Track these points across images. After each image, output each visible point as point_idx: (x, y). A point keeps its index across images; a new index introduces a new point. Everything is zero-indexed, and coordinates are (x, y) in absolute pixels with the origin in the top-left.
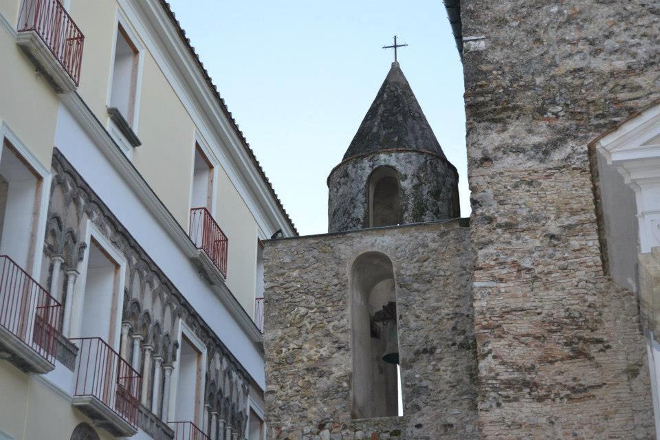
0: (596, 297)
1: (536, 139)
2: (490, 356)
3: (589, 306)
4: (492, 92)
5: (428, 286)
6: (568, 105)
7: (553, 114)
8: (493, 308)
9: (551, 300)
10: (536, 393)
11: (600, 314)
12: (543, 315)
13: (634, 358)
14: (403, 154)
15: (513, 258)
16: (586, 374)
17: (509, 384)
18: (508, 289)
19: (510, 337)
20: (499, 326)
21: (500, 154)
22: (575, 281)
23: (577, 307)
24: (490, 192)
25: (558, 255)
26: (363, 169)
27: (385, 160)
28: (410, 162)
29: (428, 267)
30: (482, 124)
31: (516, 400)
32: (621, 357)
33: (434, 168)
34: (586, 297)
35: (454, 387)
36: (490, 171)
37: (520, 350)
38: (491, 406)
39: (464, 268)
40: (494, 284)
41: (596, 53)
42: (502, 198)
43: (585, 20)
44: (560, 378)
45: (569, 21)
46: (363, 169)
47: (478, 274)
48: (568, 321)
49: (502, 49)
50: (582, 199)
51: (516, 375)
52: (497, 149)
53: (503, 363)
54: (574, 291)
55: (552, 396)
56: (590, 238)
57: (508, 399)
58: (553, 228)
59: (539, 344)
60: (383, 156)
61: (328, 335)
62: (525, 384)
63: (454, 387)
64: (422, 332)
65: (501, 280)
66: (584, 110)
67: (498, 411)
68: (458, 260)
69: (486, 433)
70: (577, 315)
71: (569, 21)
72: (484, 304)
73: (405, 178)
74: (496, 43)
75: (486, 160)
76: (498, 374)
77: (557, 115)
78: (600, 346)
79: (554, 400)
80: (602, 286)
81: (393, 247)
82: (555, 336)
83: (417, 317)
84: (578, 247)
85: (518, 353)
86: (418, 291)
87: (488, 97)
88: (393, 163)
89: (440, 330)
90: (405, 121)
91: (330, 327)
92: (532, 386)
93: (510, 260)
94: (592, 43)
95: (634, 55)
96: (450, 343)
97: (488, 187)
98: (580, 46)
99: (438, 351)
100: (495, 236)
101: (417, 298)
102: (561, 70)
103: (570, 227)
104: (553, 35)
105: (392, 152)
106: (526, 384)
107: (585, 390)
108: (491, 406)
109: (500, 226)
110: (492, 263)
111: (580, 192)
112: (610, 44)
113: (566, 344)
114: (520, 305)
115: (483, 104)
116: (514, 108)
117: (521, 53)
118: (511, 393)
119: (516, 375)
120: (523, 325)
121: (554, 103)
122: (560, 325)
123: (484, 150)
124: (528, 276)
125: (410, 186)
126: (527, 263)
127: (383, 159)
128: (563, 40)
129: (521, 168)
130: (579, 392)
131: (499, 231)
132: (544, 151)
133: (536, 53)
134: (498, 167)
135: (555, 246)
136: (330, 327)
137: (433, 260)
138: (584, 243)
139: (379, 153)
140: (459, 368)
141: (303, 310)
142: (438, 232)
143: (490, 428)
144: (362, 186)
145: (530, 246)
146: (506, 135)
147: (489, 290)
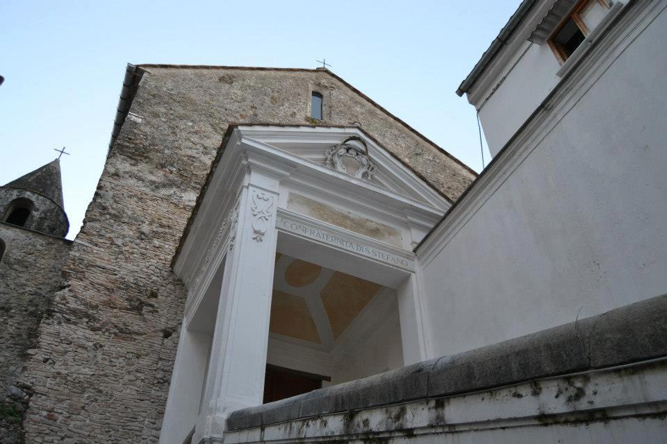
0: (159, 279)
1: (153, 178)
2: (67, 289)
3: (152, 282)
4: (136, 144)
5: (25, 270)
6: (180, 170)
7: (170, 170)
8: (83, 260)
9: (126, 271)
10: (91, 324)
11: (158, 290)
12: (118, 276)
13: (172, 324)
14: (42, 198)
15: (111, 236)
17: (74, 312)
18: (99, 252)
19: (88, 282)
20: (83, 272)
21: (127, 176)
22: (148, 264)
24: (111, 193)
25: (142, 245)
26: (11, 195)
27: (29, 196)
28: (45, 204)
29: (31, 259)
30: (122, 156)
31: (75, 324)
32: (163, 320)
34: (152, 276)
35: (13, 337)
36: (116, 182)
37: (91, 292)
38: (53, 322)
39: (55, 268)
40: (90, 245)
42: (117, 199)
43: (205, 136)
44: (114, 320)
45: (196, 133)
46: (11, 195)
48: (134, 286)
49: (151, 128)
50: (170, 220)
51: (82, 307)
53: (75, 297)
54: (145, 270)
55: (104, 330)
56: (168, 243)
57: (68, 321)
58: (146, 228)
59: (107, 293)
60: (28, 193)
62: (85, 315)
63: (13, 337)
64: (6, 296)
65: (96, 245)
66: (189, 176)
67: (57, 327)
68: (52, 262)
69: (41, 340)
70: (142, 284)
71: (196, 133)
72: (78, 255)
73: (38, 210)
74: (148, 123)
75: (116, 175)
76: (68, 303)
77: (171, 172)
78: (151, 309)
79: (104, 333)
80: (165, 273)
81: (11, 238)
83: (8, 285)
84: (158, 245)
85: (90, 295)
86: (16, 270)
87: (132, 146)
89: (19, 298)
90: (51, 185)
92: (91, 318)
93: (108, 235)
96: (24, 309)
97: (111, 190)
98: (198, 146)
99: (13, 311)
100: (103, 219)
101: (13, 274)
102: (183, 153)
103: (156, 233)
104: (184, 134)
105: (36, 193)
106: (87, 315)
107: (130, 333)
108: (53, 322)
109: (109, 214)
110: (95, 233)
111: (171, 216)
113: (127, 299)
114: (103, 265)
116: (146, 158)
117: (162, 135)
118: (73, 318)
119: (82, 307)
120: (101, 278)
121: (172, 165)
123: (118, 169)
124: (116, 249)
125: (38, 216)
126: (119, 242)
127: (28, 194)
128: (189, 139)
129: (137, 188)
130: (124, 333)
131: (108, 216)
132: (156, 186)
133: (171, 138)
134: (122, 182)
135: (142, 239)
137: (36, 256)
138: (162, 244)
139: (26, 190)
140: (22, 327)
142: (47, 241)
143: (45, 337)
144: (5, 204)
145: (125, 233)
146: (135, 168)
147: (85, 248)
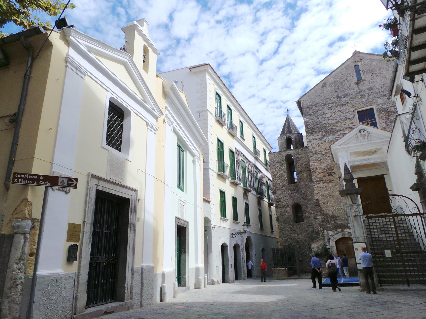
1: (318, 137)
9: (324, 166)
16: (331, 178)
17: (318, 181)
37: (319, 175)
41: (329, 120)
88: (290, 136)
106: (321, 181)
112: (331, 118)
120: (320, 171)
121: (322, 130)
126: (319, 160)
130: (331, 181)
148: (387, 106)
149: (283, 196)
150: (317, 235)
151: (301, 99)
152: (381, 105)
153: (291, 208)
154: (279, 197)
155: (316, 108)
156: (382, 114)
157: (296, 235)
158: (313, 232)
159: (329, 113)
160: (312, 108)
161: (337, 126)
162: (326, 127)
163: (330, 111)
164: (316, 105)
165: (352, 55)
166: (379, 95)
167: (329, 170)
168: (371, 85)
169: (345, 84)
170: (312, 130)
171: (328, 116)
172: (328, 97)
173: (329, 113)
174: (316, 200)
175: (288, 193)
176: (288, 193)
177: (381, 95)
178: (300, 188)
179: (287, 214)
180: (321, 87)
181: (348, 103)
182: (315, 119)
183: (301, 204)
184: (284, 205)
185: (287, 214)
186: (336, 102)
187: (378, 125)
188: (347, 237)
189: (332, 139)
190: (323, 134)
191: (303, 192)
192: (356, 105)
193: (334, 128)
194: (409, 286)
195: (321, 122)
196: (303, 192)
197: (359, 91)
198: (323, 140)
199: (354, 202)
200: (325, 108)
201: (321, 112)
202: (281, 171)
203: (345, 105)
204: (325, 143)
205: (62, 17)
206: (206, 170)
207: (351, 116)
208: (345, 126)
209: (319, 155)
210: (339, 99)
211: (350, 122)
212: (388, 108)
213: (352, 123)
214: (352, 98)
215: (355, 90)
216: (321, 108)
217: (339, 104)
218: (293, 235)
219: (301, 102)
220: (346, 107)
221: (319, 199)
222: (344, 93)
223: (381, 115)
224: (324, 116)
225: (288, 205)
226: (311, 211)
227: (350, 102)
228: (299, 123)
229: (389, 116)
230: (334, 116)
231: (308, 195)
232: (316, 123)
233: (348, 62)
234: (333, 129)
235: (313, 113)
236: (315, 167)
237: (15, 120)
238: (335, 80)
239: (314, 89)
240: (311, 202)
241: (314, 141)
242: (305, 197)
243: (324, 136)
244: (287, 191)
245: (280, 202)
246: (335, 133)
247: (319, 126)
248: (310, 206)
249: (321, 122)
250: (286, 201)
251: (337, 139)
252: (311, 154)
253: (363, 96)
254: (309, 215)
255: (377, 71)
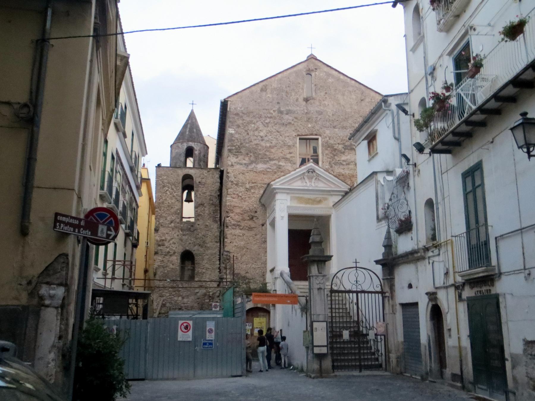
1: (244, 162)
9: (245, 205)
13: (264, 222)
16: (252, 224)
17: (234, 225)
23: (251, 208)
29: (204, 181)
32: (261, 221)
33: (204, 148)
37: (237, 217)
41: (262, 140)
47: (228, 196)
52: (235, 163)
61: (174, 196)
77: (251, 156)
82: (246, 214)
88: (193, 146)
91: (175, 194)
92: (239, 226)
94: (262, 137)
95: (271, 143)
102: (253, 144)
103: (252, 187)
106: (238, 225)
112: (266, 139)
115: (233, 149)
118: (234, 227)
120: (238, 211)
121: (250, 152)
122: (247, 211)
123: (232, 163)
126: (240, 194)
130: (250, 229)
136: (175, 194)
141: (167, 189)
146: (237, 159)
148: (335, 141)
149: (169, 238)
150: (210, 300)
151: (229, 99)
152: (328, 139)
153: (179, 257)
154: (163, 238)
155: (248, 119)
156: (327, 150)
157: (180, 298)
158: (205, 295)
159: (264, 131)
160: (242, 117)
161: (272, 152)
162: (256, 149)
163: (266, 128)
164: (248, 113)
165: (306, 59)
166: (328, 124)
167: (251, 211)
168: (322, 108)
169: (291, 95)
170: (237, 149)
171: (262, 134)
172: (267, 108)
173: (264, 131)
174: (228, 252)
175: (178, 233)
176: (178, 233)
177: (331, 125)
178: (196, 230)
179: (171, 266)
180: (259, 90)
181: (290, 123)
182: (244, 135)
183: (194, 253)
184: (169, 252)
185: (171, 266)
186: (275, 118)
187: (320, 163)
188: (259, 308)
189: (261, 169)
190: (252, 159)
191: (200, 235)
192: (300, 130)
193: (267, 153)
194: (360, 371)
195: (251, 141)
196: (200, 235)
197: (306, 111)
198: (250, 167)
199: (320, 272)
200: (259, 122)
201: (253, 125)
202: (171, 199)
203: (286, 125)
204: (252, 173)
205: (375, 128)
206: (97, 188)
207: (291, 143)
208: (282, 155)
209: (241, 188)
210: (279, 115)
211: (288, 151)
212: (335, 144)
213: (290, 153)
214: (296, 118)
215: (302, 109)
216: (255, 121)
217: (279, 121)
218: (176, 298)
219: (229, 103)
220: (287, 129)
221: (231, 251)
222: (287, 108)
223: (327, 152)
224: (256, 133)
225: (174, 253)
226: (207, 266)
227: (293, 123)
228: (209, 130)
229: (334, 155)
230: (270, 137)
231: (207, 241)
232: (244, 140)
233: (300, 67)
234: (266, 155)
235: (243, 124)
236: (233, 204)
237: (28, 117)
238: (279, 85)
239: (250, 89)
240: (209, 252)
241: (238, 167)
242: (201, 243)
243: (252, 162)
244: (176, 230)
245: (163, 245)
246: (267, 161)
247: (247, 145)
248: (207, 257)
249: (251, 141)
250: (173, 245)
251: (268, 170)
252: (230, 183)
253: (310, 120)
254: (204, 271)
255: (332, 91)
